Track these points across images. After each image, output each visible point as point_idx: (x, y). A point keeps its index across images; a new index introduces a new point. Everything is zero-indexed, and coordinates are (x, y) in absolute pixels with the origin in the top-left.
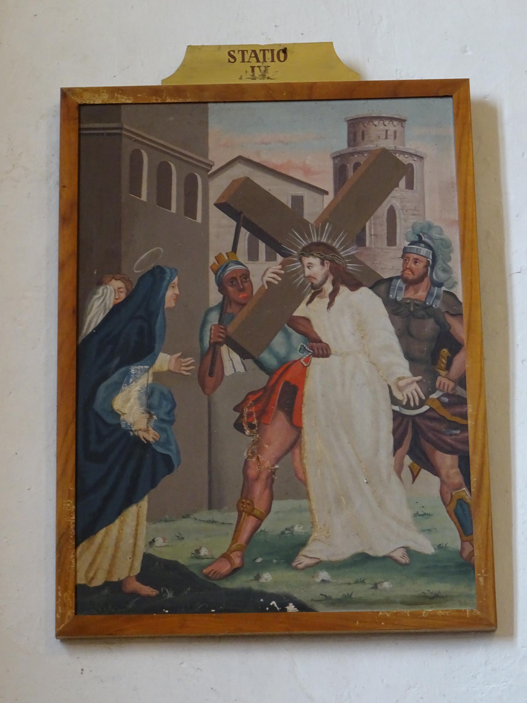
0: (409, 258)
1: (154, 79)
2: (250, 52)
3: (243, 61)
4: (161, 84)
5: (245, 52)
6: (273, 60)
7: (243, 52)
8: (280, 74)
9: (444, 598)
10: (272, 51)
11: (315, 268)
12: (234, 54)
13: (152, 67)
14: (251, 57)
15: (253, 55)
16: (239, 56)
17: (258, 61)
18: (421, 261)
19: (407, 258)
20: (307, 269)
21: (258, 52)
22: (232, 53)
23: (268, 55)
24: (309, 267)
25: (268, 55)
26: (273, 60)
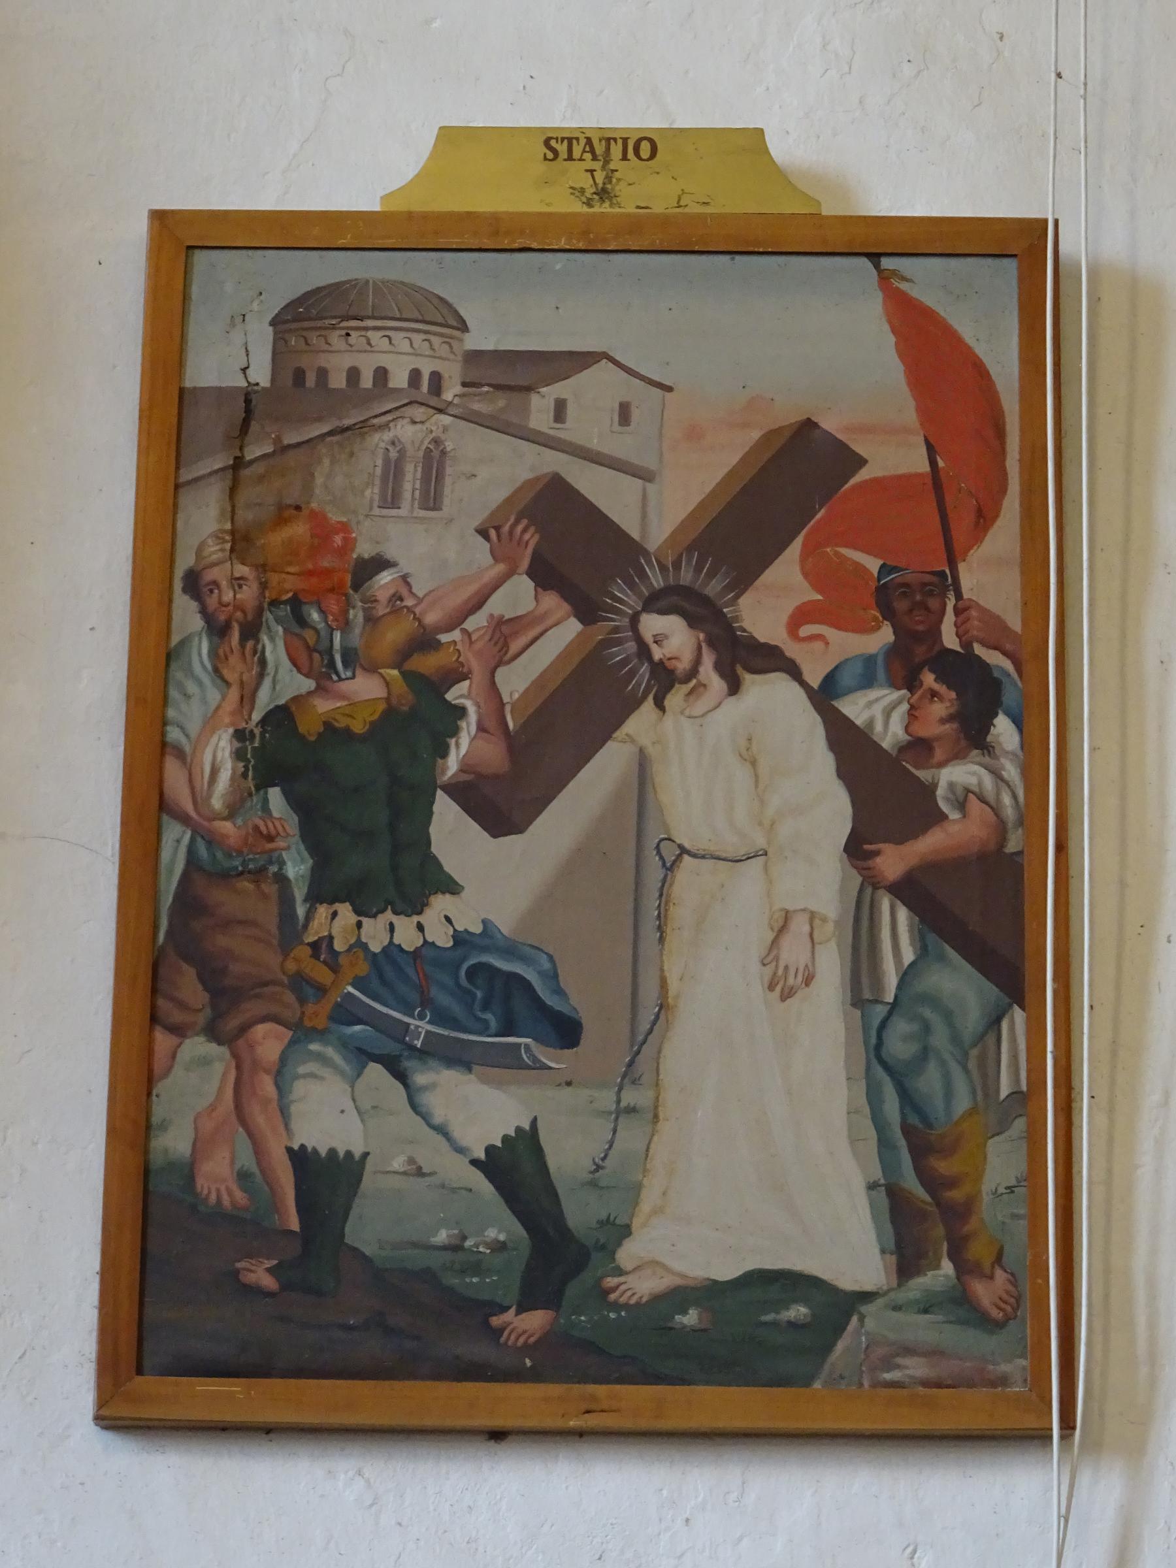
0: (215, 583)
1: (367, 200)
2: (583, 142)
3: (570, 158)
4: (378, 208)
5: (575, 142)
6: (625, 158)
7: (570, 140)
8: (643, 192)
9: (949, 1323)
10: (625, 141)
11: (672, 637)
12: (558, 146)
13: (362, 166)
14: (584, 151)
15: (587, 149)
16: (562, 148)
17: (595, 158)
18: (941, 699)
19: (209, 584)
20: (654, 648)
21: (595, 142)
22: (553, 143)
23: (616, 150)
24: (656, 642)
25: (616, 150)
26: (625, 158)
